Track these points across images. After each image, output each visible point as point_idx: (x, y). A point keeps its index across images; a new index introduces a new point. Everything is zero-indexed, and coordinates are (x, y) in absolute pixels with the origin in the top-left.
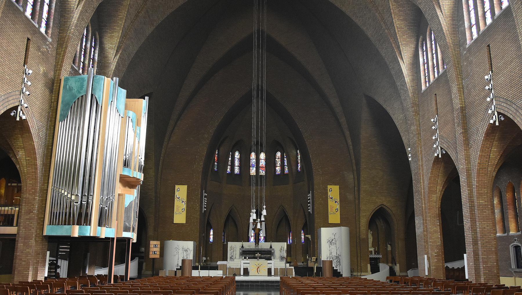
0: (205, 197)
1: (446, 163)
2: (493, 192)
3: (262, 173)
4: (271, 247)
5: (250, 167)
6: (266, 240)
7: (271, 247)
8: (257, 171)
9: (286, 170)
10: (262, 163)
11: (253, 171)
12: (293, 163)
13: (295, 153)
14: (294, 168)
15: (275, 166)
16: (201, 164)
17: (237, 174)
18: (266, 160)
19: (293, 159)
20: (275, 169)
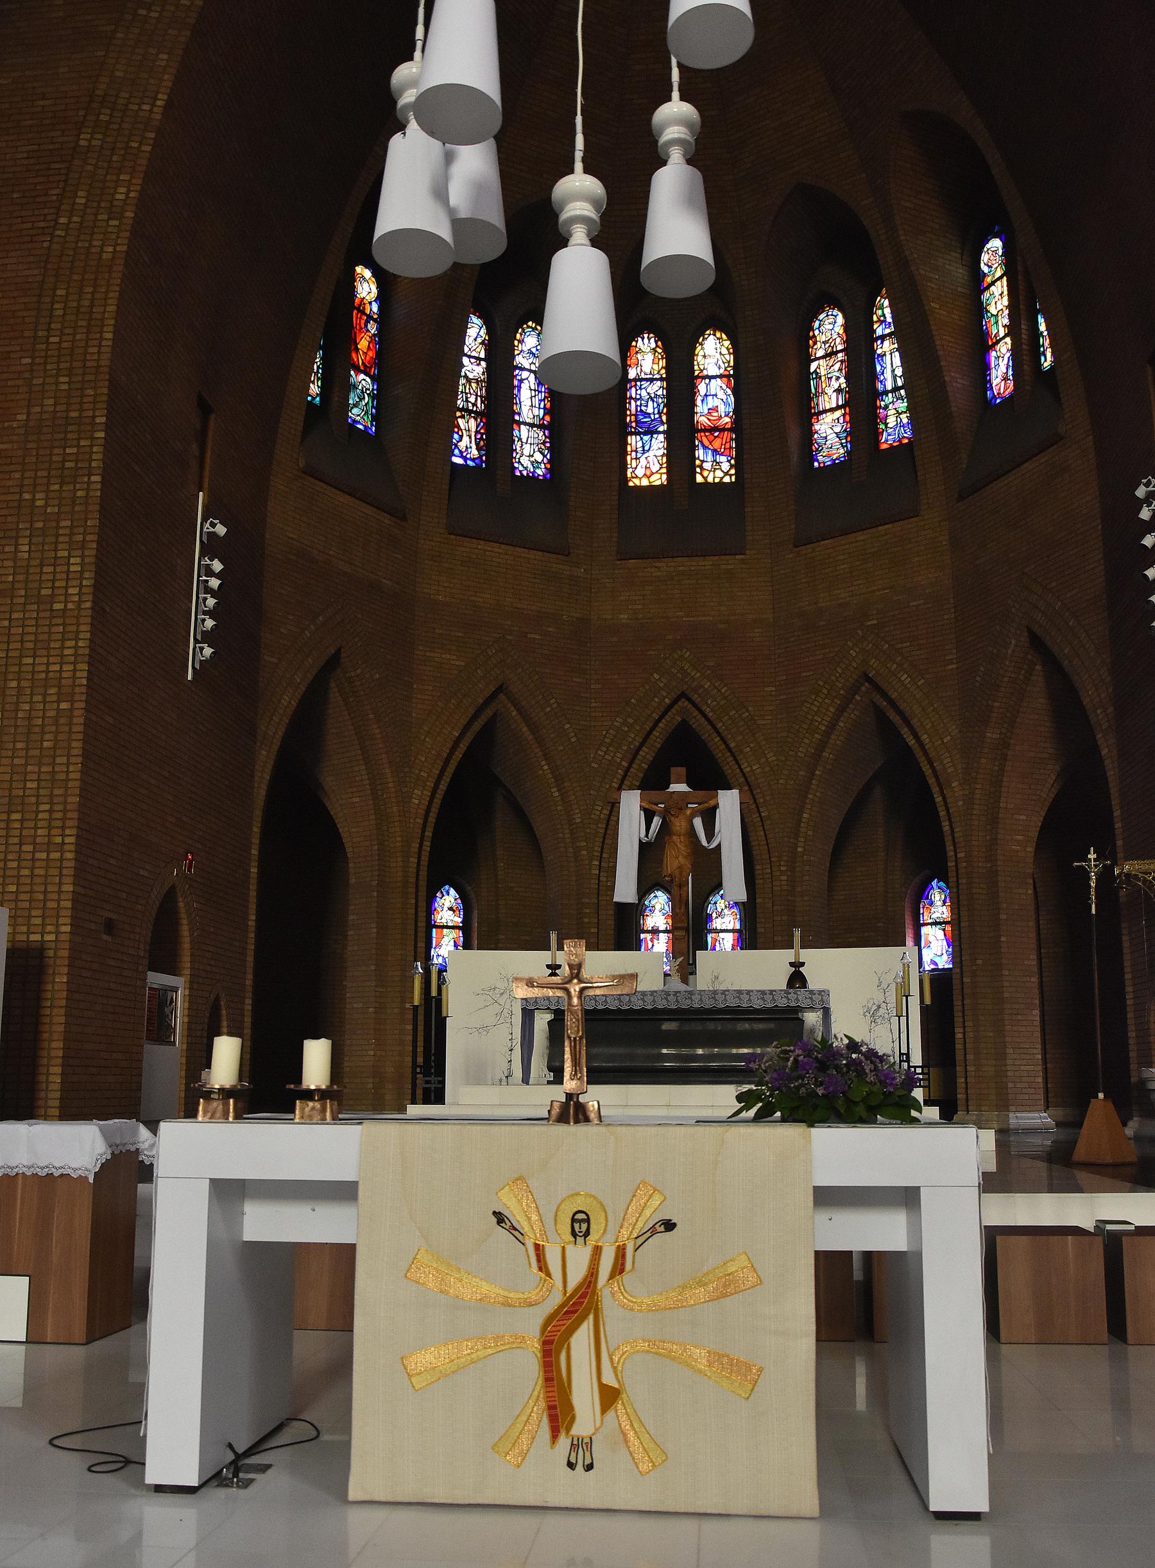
0: (212, 547)
1: (269, 1466)
2: (915, 1121)
3: (715, 467)
4: (797, 979)
5: (624, 432)
6: (748, 938)
7: (797, 979)
8: (680, 457)
9: (896, 420)
10: (715, 401)
11: (647, 463)
12: (949, 345)
13: (959, 273)
14: (957, 381)
15: (808, 414)
16: (126, 192)
17: (532, 479)
18: (739, 379)
19: (944, 315)
20: (808, 433)
